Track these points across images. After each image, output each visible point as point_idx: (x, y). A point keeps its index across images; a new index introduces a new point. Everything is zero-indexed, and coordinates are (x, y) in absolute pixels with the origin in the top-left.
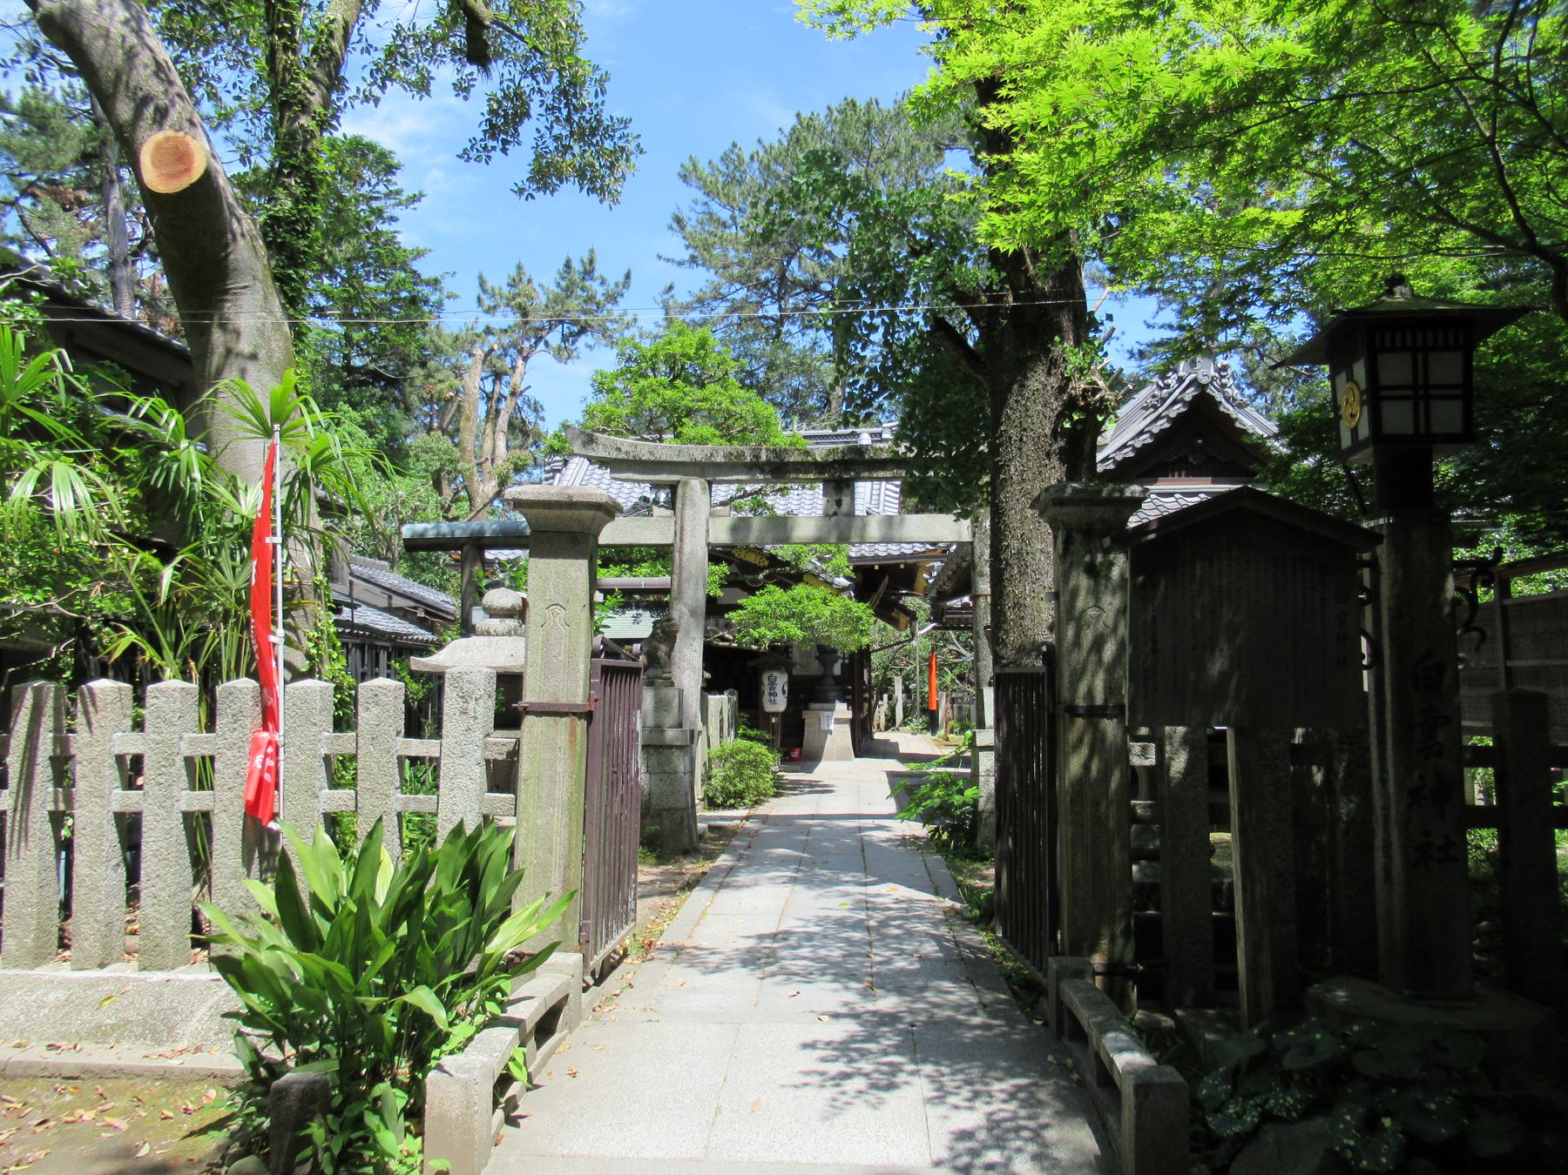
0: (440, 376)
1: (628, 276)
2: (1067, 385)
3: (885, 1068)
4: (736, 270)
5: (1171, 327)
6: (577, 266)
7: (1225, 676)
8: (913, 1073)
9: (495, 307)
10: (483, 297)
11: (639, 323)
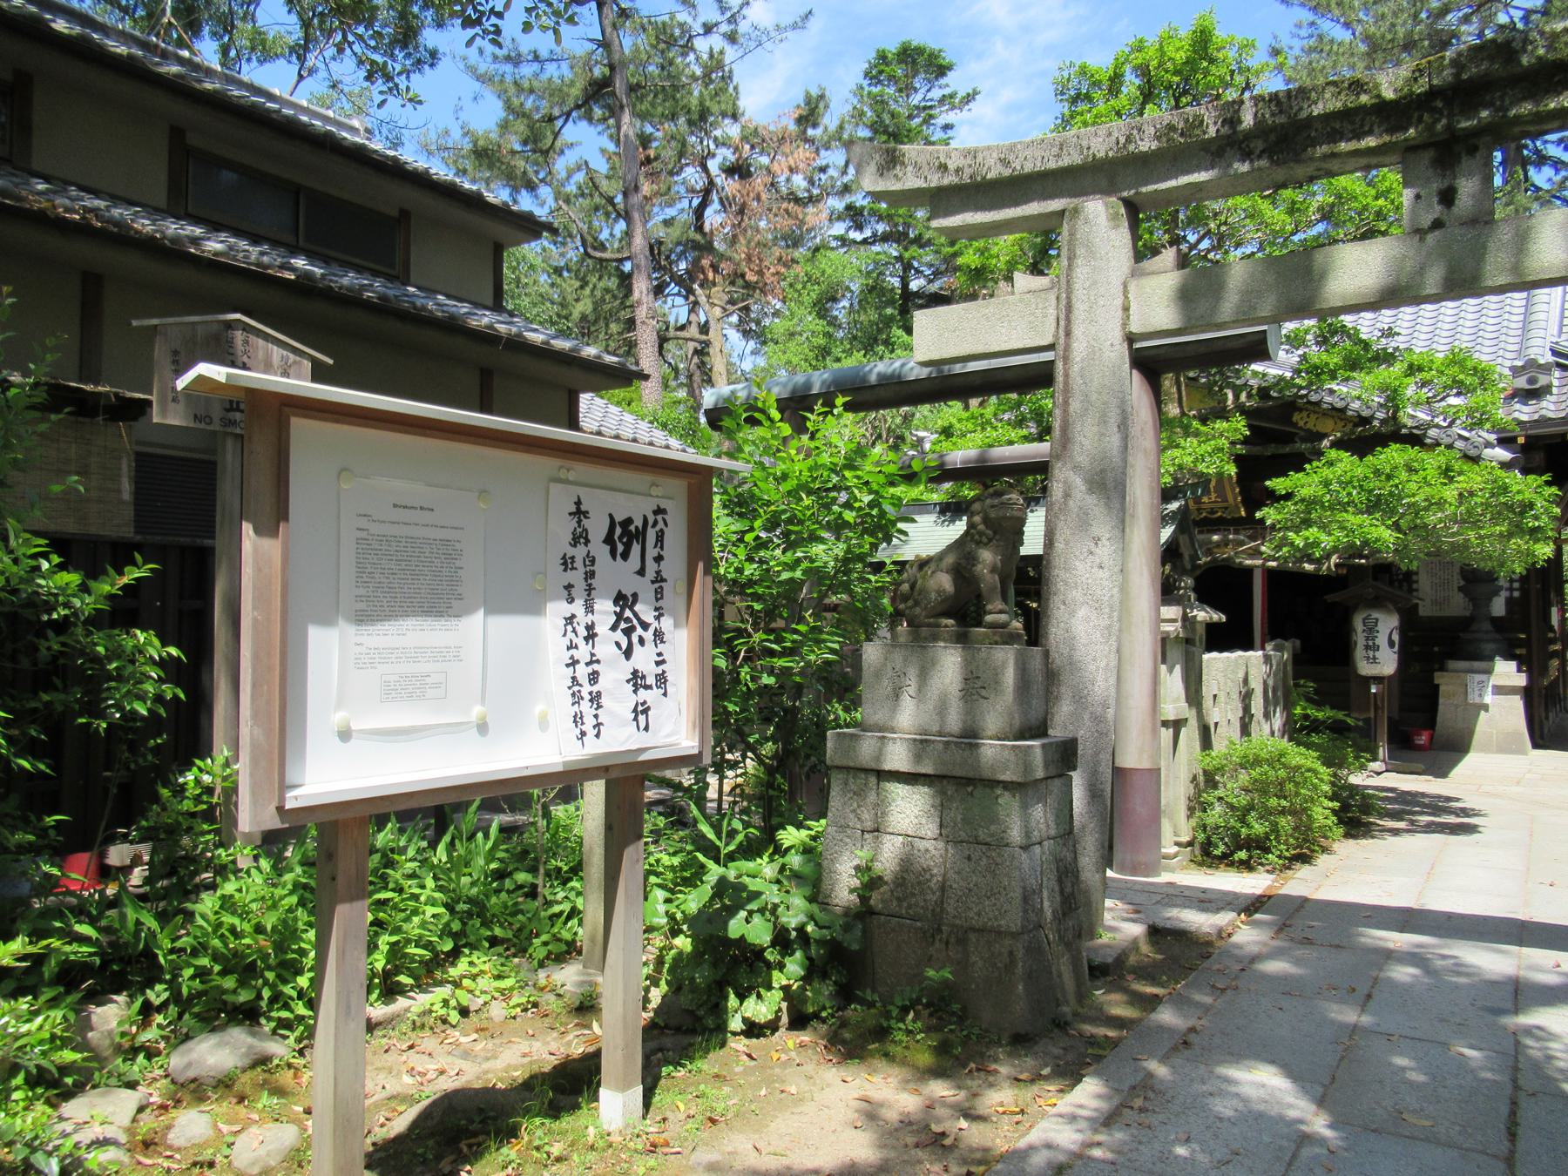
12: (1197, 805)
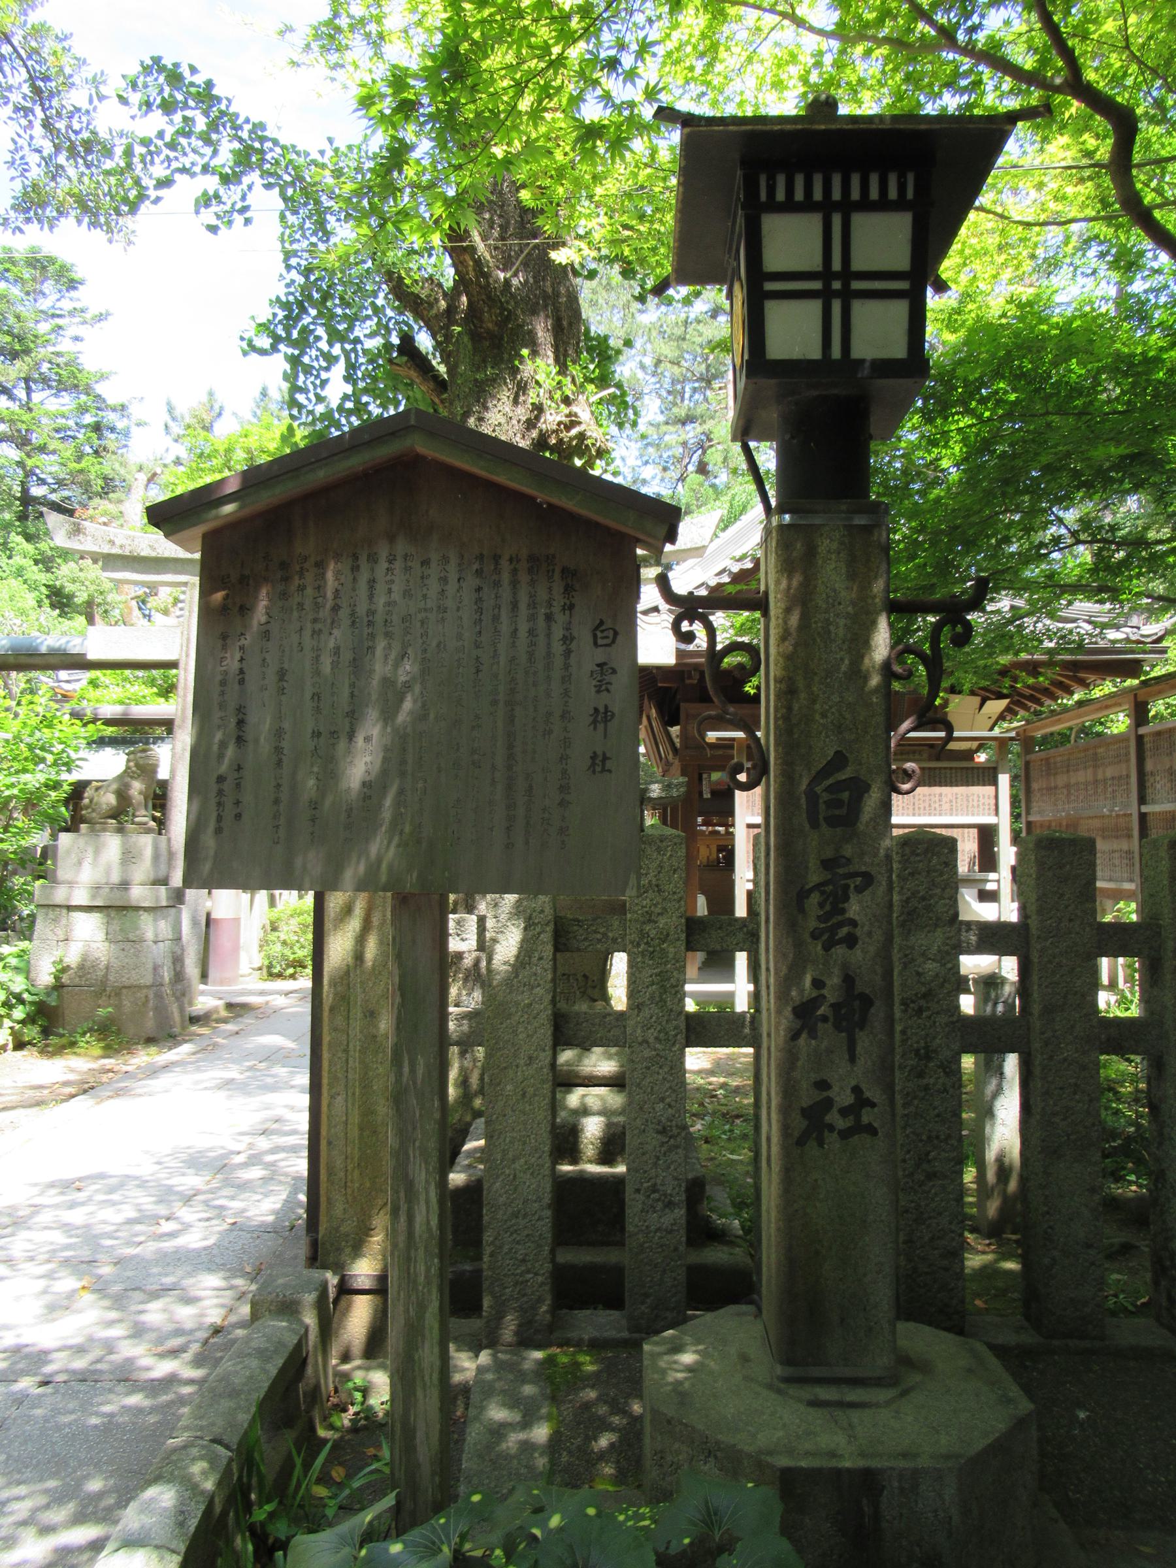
2: (537, 418)
7: (372, 789)
10: (171, 423)
12: (264, 943)
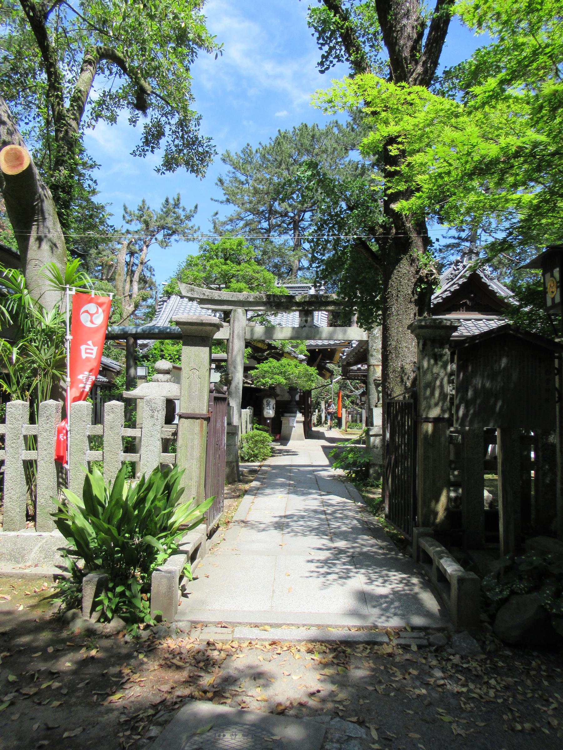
0: (104, 253)
1: (196, 207)
2: (419, 271)
3: (344, 571)
4: (248, 206)
5: (454, 238)
6: (171, 201)
8: (357, 573)
9: (131, 221)
10: (126, 215)
11: (201, 230)
